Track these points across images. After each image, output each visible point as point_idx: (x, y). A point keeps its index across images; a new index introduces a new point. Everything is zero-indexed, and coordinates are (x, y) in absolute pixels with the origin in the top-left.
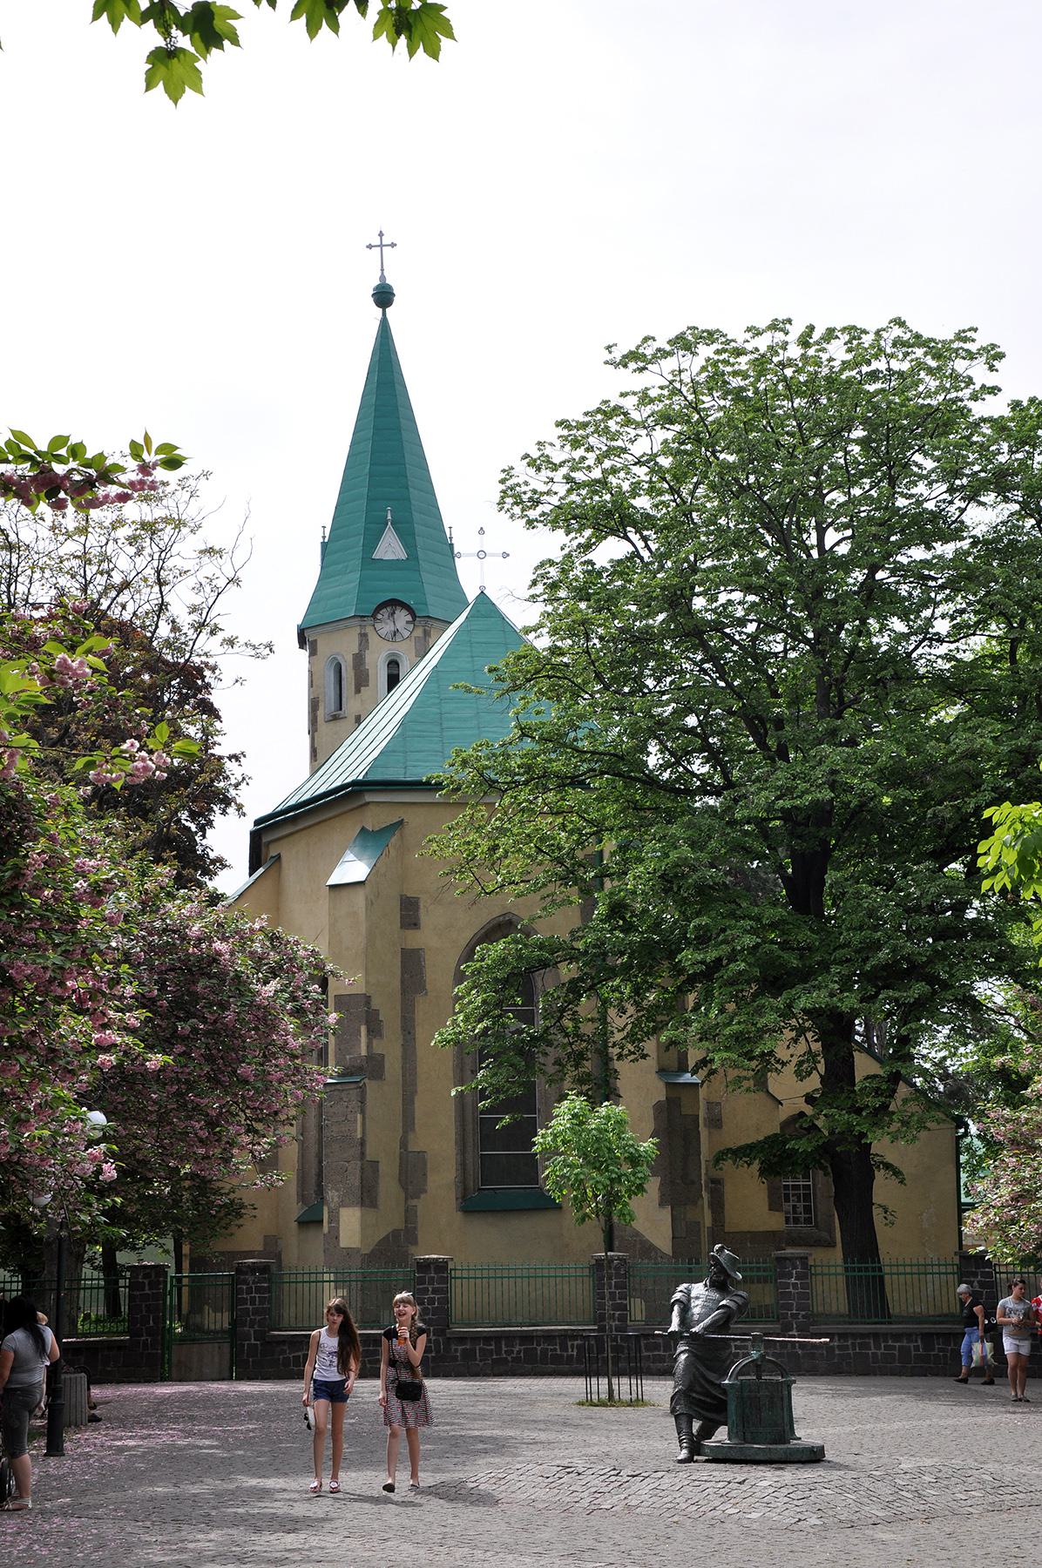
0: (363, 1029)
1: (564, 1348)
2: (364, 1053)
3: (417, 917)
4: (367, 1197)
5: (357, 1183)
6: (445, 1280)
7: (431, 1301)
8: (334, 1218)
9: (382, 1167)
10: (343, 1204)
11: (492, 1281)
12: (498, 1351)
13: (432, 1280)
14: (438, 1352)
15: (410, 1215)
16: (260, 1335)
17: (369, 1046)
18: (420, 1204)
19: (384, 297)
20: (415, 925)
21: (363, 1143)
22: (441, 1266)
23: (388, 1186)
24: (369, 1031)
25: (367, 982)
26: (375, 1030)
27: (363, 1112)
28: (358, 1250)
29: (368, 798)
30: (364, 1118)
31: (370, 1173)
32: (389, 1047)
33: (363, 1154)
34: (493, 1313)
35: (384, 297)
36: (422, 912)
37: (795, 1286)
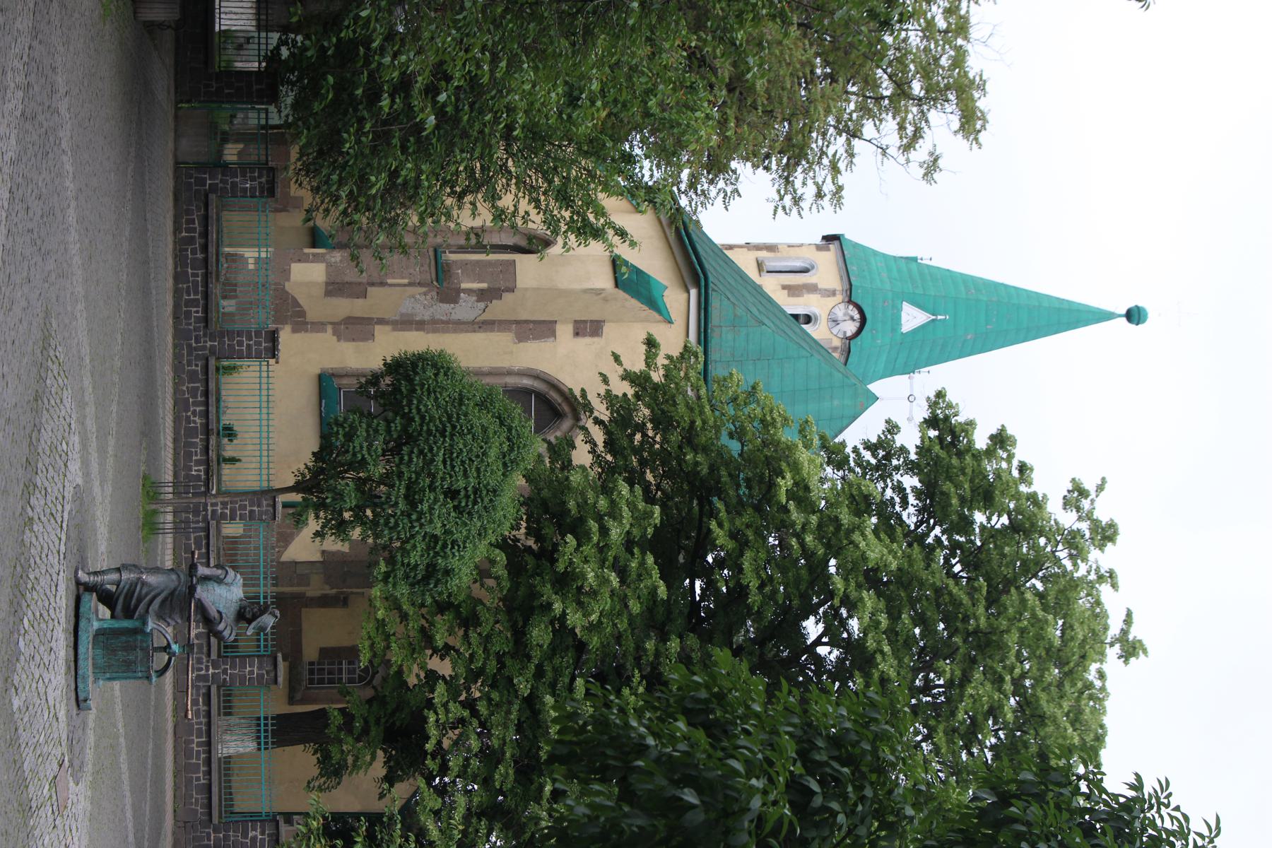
0: (484, 285)
1: (198, 463)
2: (463, 286)
3: (584, 335)
4: (335, 288)
5: (347, 279)
6: (258, 356)
7: (240, 343)
8: (316, 259)
9: (360, 301)
10: (329, 265)
11: (257, 398)
12: (195, 404)
13: (259, 344)
14: (196, 349)
15: (319, 326)
16: (213, 188)
17: (469, 292)
18: (328, 336)
19: (1134, 315)
20: (577, 334)
21: (383, 284)
22: (273, 352)
23: (344, 307)
24: (482, 291)
25: (526, 289)
26: (483, 295)
27: (410, 284)
28: (288, 279)
29: (693, 292)
30: (405, 285)
31: (358, 291)
32: (466, 309)
33: (373, 284)
34: (231, 399)
35: (1134, 315)
36: (588, 340)
37: (251, 672)
